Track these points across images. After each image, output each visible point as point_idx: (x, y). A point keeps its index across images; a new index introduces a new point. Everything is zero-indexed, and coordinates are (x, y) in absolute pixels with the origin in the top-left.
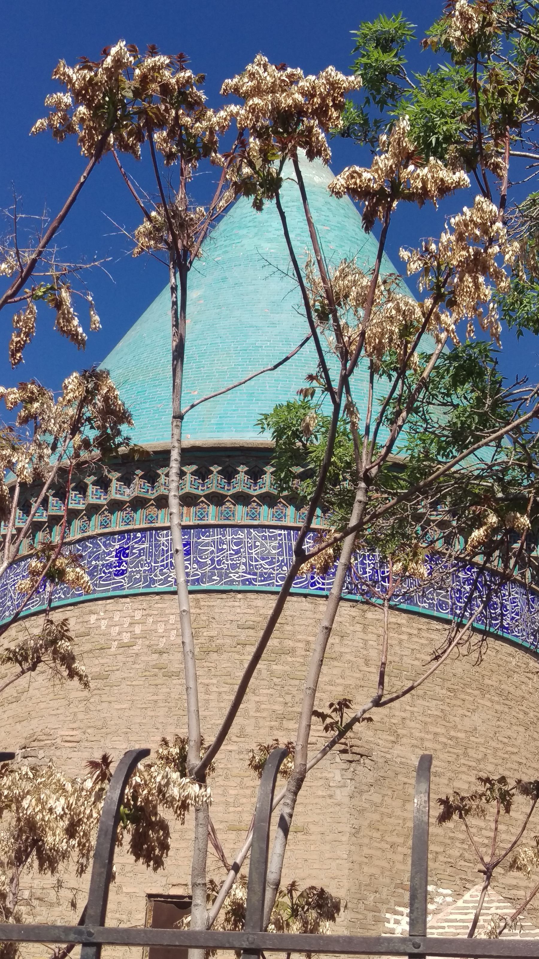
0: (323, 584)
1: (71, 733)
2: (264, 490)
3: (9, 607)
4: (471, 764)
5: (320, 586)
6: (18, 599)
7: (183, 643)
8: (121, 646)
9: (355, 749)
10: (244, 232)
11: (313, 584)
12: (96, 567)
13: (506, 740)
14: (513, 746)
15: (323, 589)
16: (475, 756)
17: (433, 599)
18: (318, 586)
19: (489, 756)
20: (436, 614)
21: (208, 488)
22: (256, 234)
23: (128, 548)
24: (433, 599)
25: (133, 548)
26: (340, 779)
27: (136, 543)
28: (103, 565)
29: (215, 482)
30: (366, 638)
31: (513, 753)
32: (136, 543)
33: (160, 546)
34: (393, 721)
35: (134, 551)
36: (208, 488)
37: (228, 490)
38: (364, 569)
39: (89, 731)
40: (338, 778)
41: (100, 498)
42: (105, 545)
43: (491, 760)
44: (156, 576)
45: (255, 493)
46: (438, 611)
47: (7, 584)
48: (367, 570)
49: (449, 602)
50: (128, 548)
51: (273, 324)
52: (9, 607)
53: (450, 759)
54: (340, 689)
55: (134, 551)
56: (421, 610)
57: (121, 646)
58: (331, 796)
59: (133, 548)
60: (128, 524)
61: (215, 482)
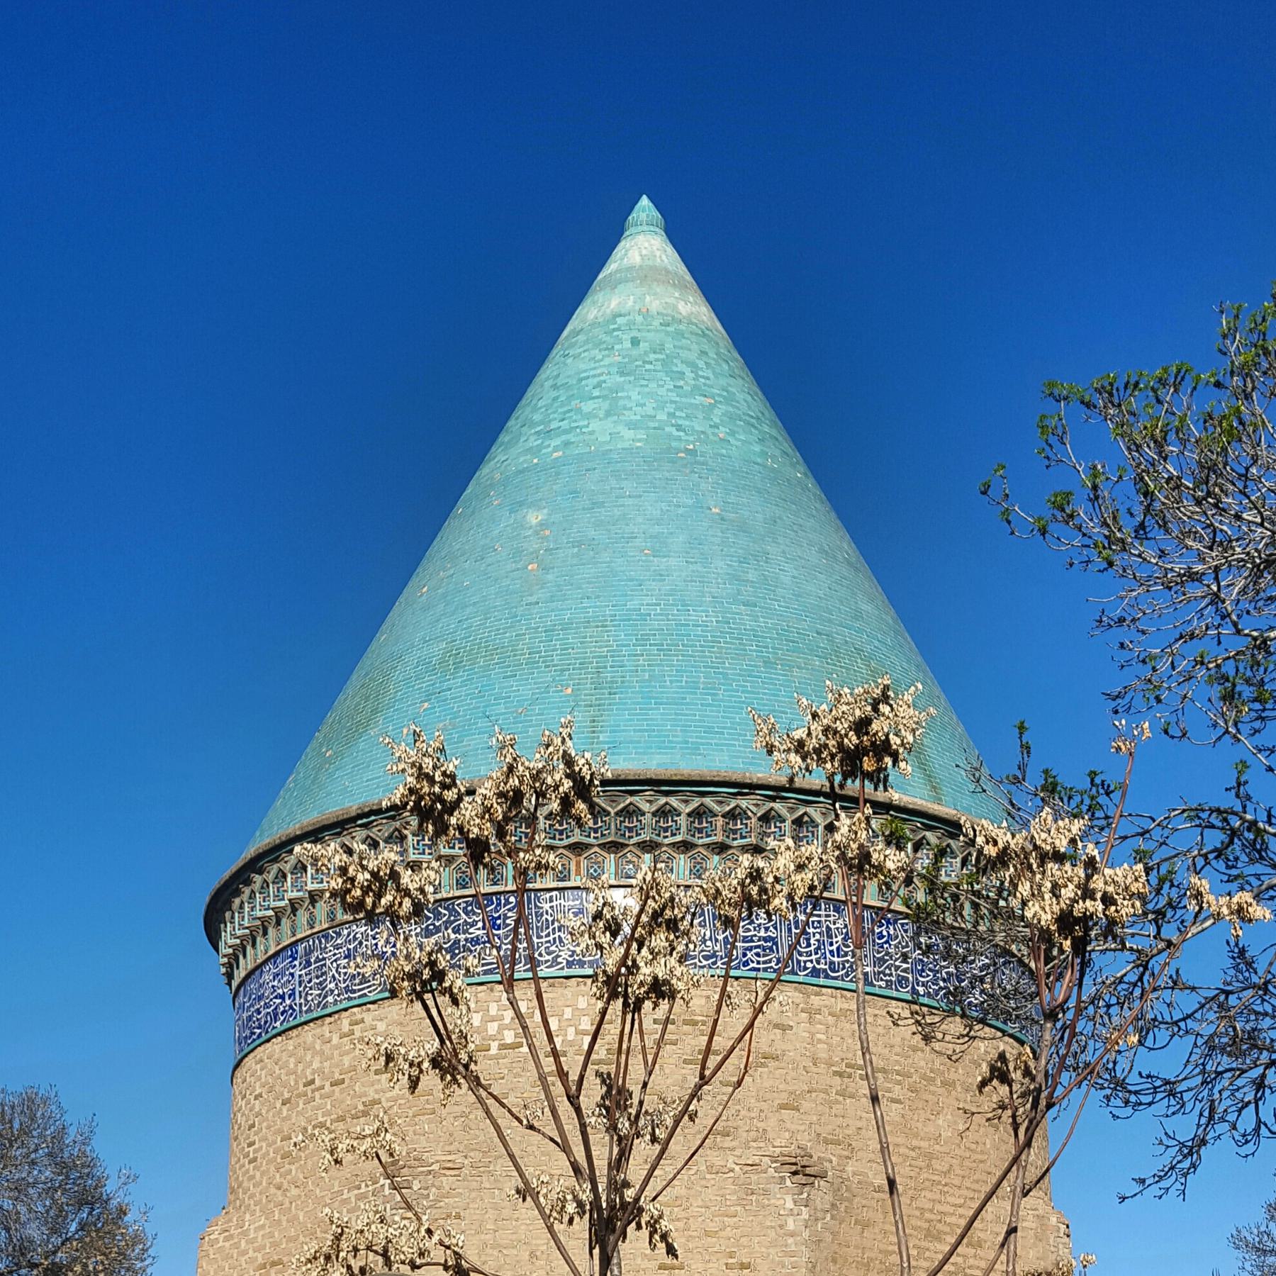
0: (758, 963)
1: (449, 1158)
2: (679, 838)
3: (332, 991)
4: (936, 1178)
5: (755, 965)
6: (345, 981)
7: (892, 1183)
8: (503, 1047)
9: (808, 1171)
10: (588, 407)
11: (746, 964)
12: (457, 942)
13: (974, 1146)
14: (982, 1152)
15: (758, 970)
16: (939, 1167)
17: (891, 975)
18: (752, 965)
19: (955, 1167)
20: (895, 994)
21: (603, 835)
22: (608, 414)
23: (499, 918)
24: (891, 975)
25: (506, 917)
26: (792, 1206)
27: (509, 910)
28: (466, 940)
29: (613, 827)
30: (813, 1030)
31: (982, 1162)
32: (509, 910)
33: (542, 915)
34: (847, 1132)
35: (508, 921)
36: (603, 835)
37: (630, 837)
38: (808, 940)
39: (472, 1154)
40: (790, 1205)
41: (453, 848)
42: (467, 913)
43: (958, 1172)
44: (540, 955)
45: (666, 841)
46: (897, 990)
47: (324, 959)
48: (812, 941)
49: (910, 976)
50: (499, 918)
51: (660, 576)
52: (332, 991)
53: (912, 1174)
54: (785, 1095)
55: (508, 921)
56: (877, 991)
57: (503, 1047)
58: (781, 1227)
59: (506, 917)
60: (495, 884)
61: (613, 827)
